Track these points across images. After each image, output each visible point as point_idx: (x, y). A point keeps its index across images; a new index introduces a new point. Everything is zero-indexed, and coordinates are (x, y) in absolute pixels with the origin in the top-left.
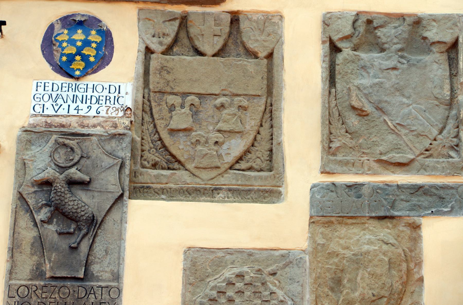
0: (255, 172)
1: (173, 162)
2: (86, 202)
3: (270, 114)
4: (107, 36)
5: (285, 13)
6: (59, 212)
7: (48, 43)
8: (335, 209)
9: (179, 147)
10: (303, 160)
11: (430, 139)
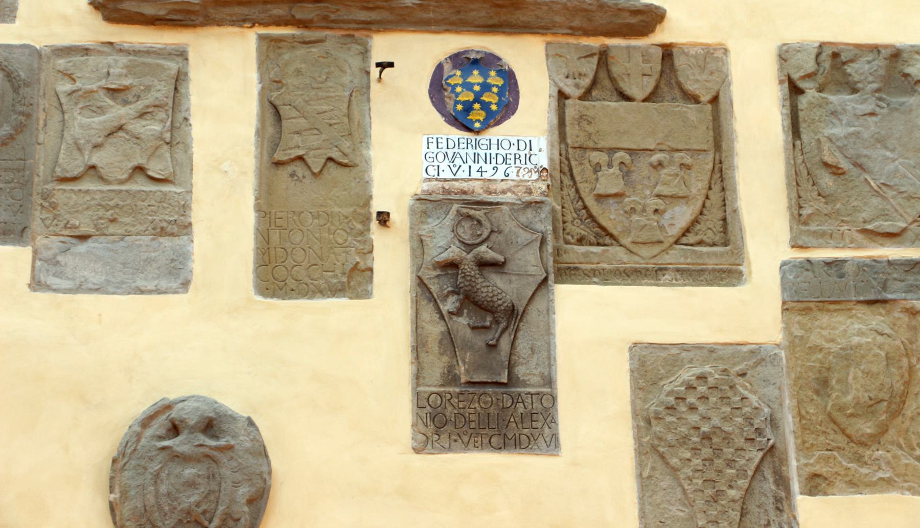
0: (708, 249)
2: (501, 288)
3: (721, 175)
6: (471, 301)
7: (438, 88)
8: (811, 292)
9: (610, 216)
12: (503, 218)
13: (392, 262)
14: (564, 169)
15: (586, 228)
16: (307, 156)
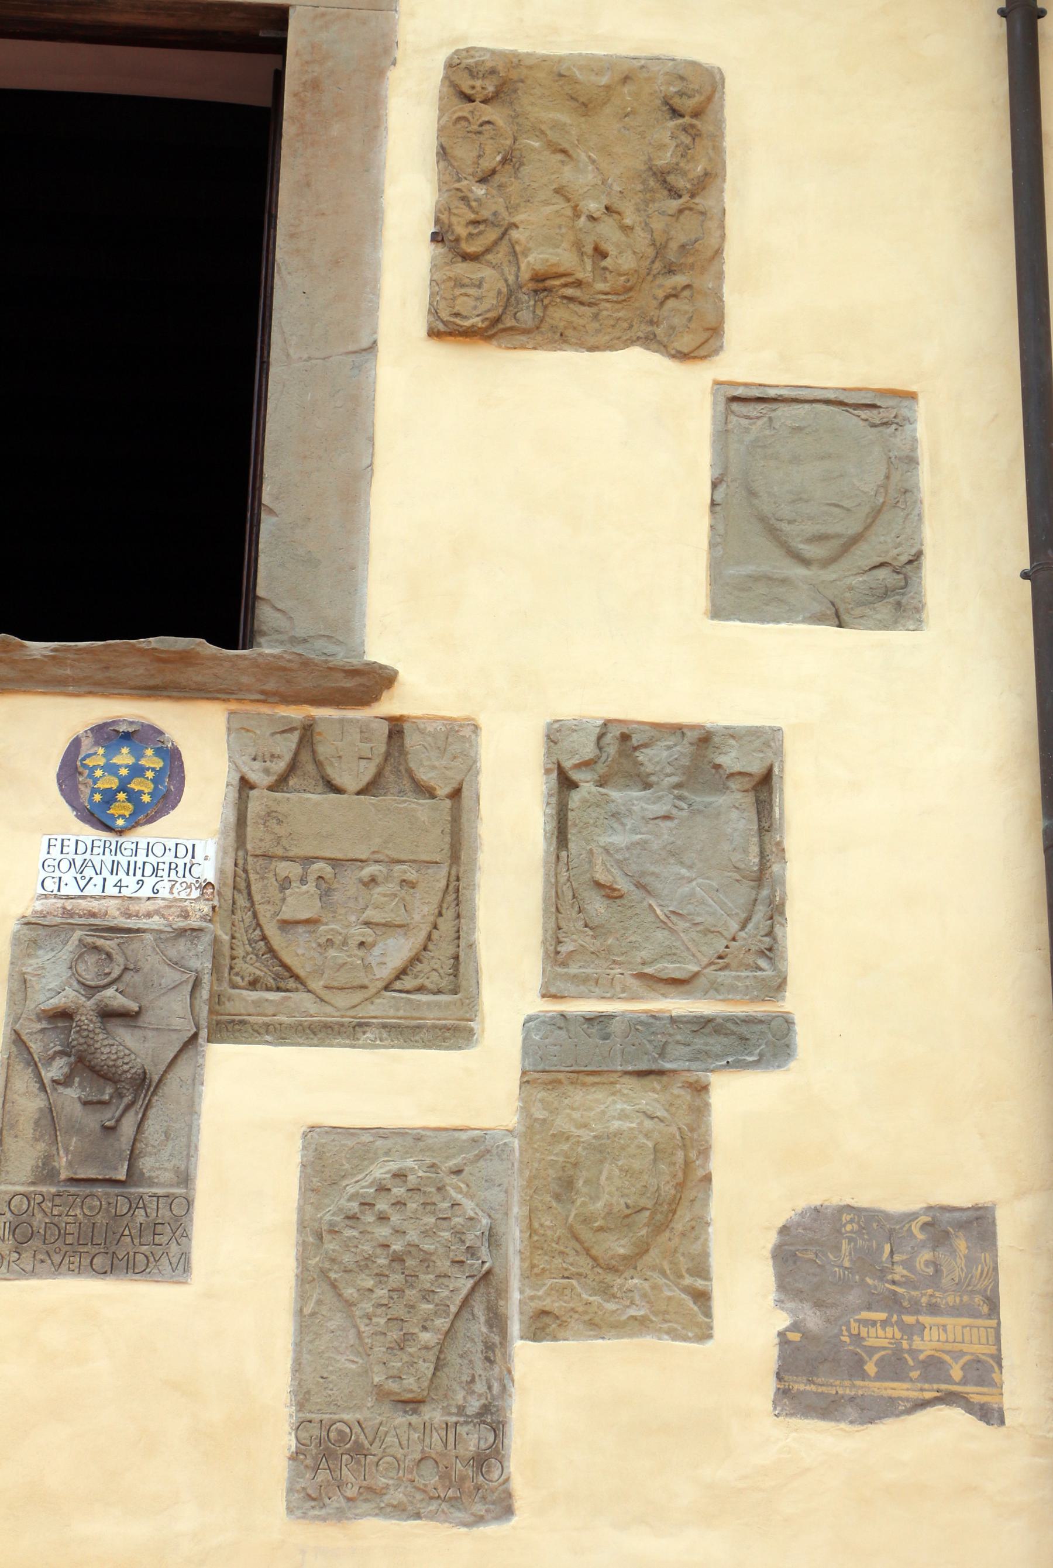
0: (431, 997)
1: (287, 977)
2: (133, 1048)
4: (173, 758)
6: (85, 1065)
7: (71, 772)
8: (559, 1060)
9: (297, 951)
12: (145, 951)
14: (239, 885)
15: (257, 968)
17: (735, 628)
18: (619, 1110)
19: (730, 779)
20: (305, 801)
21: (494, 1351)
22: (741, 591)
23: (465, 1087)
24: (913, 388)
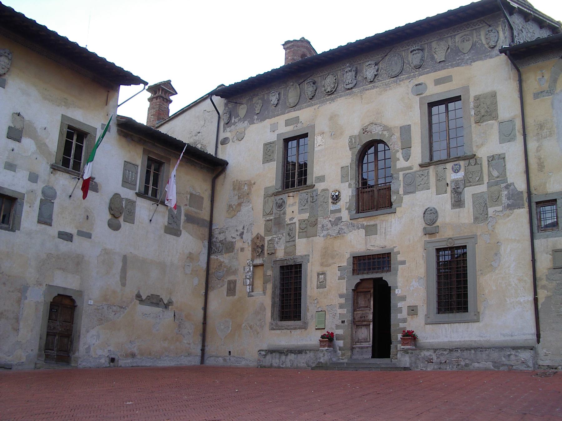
0: (480, 181)
1: (470, 182)
2: (460, 190)
3: (482, 173)
4: (460, 165)
5: (162, 231)
6: (456, 192)
7: (453, 168)
8: (490, 185)
9: (471, 180)
10: (486, 179)
11: (298, 159)
12: (459, 182)
13: (449, 189)
14: (465, 174)
15: (467, 182)
16: (440, 179)
17: (166, 79)
18: (495, 188)
19: (502, 157)
20: (470, 167)
21: (487, 209)
22: (502, 141)
23: (483, 188)
24: (417, 305)
